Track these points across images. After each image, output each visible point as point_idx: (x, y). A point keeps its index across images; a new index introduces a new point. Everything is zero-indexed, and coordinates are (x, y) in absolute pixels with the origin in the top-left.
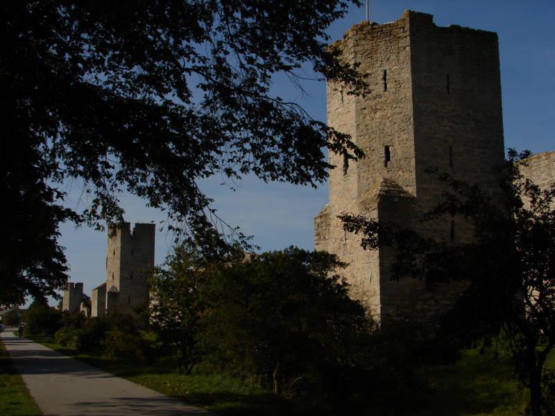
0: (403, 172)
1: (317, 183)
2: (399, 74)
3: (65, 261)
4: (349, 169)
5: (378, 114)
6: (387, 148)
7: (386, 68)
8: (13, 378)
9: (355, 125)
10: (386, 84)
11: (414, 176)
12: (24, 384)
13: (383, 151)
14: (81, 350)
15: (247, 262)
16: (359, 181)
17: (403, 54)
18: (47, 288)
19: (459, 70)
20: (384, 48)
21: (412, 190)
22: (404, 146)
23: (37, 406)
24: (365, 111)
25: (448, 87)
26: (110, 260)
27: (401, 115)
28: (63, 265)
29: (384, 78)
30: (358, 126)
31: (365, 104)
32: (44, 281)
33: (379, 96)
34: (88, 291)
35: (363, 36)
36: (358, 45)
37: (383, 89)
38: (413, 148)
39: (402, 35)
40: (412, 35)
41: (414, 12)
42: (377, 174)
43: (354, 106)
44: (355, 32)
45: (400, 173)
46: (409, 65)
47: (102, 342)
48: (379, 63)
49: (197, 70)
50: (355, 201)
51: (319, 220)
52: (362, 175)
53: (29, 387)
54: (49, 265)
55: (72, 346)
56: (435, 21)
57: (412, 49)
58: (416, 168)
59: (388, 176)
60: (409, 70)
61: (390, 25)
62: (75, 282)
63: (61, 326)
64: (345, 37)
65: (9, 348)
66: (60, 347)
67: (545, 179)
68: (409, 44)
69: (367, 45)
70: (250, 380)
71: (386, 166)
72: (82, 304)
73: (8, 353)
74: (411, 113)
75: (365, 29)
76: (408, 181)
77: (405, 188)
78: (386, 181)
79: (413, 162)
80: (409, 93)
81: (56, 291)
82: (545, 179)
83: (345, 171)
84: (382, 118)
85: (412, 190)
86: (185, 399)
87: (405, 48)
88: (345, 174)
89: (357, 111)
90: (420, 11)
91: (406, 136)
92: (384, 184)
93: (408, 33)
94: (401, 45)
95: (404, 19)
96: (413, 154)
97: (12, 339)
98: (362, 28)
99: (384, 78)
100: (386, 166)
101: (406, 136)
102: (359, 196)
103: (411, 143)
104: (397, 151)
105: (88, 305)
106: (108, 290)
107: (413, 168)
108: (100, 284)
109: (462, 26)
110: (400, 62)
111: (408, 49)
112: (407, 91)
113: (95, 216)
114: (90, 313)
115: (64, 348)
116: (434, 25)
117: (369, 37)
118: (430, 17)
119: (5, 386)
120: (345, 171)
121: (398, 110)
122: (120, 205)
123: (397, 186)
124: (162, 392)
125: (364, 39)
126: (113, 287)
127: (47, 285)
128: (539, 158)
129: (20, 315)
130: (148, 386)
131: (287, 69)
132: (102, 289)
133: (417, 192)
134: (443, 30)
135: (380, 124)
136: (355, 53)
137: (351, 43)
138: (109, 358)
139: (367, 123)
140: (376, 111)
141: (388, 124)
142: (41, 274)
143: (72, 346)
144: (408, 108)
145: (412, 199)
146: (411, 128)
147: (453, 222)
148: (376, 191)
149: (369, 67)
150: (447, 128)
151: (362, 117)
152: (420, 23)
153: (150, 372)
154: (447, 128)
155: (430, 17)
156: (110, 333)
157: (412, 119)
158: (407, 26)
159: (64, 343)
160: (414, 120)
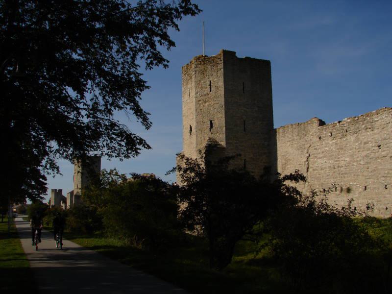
2: (217, 83)
4: (192, 132)
5: (207, 104)
6: (211, 122)
7: (211, 79)
8: (16, 240)
9: (195, 109)
10: (211, 88)
11: (224, 136)
13: (209, 123)
15: (17, 204)
18: (36, 195)
20: (210, 69)
21: (223, 143)
22: (220, 120)
24: (200, 102)
26: (75, 177)
27: (218, 105)
28: (45, 182)
29: (210, 85)
30: (196, 110)
33: (208, 94)
34: (65, 194)
36: (197, 67)
38: (224, 121)
39: (219, 62)
40: (224, 63)
41: (225, 50)
43: (194, 99)
45: (218, 134)
48: (208, 77)
49: (85, 109)
52: (198, 135)
54: (38, 182)
57: (224, 70)
58: (226, 133)
59: (211, 136)
60: (223, 81)
63: (46, 214)
64: (191, 63)
65: (17, 226)
67: (291, 138)
68: (222, 67)
69: (201, 67)
71: (210, 131)
72: (62, 202)
73: (16, 229)
74: (223, 103)
76: (222, 141)
77: (220, 143)
78: (210, 139)
79: (224, 129)
80: (223, 93)
81: (41, 196)
82: (291, 138)
84: (208, 106)
85: (223, 143)
87: (220, 69)
88: (191, 134)
89: (196, 103)
91: (221, 115)
93: (222, 61)
96: (224, 125)
99: (210, 85)
100: (210, 131)
102: (196, 147)
103: (224, 119)
104: (216, 123)
105: (65, 202)
107: (224, 133)
110: (218, 76)
111: (222, 70)
112: (222, 92)
113: (46, 168)
114: (66, 207)
115: (47, 226)
116: (236, 57)
117: (202, 63)
118: (235, 53)
119: (11, 243)
120: (191, 133)
121: (217, 102)
122: (57, 165)
123: (216, 141)
124: (80, 244)
125: (200, 64)
126: (77, 192)
127: (36, 193)
128: (288, 127)
129: (26, 208)
132: (72, 193)
133: (226, 144)
134: (241, 59)
135: (208, 109)
136: (196, 71)
137: (193, 66)
140: (205, 102)
141: (212, 109)
144: (222, 100)
145: (224, 148)
148: (204, 144)
149: (202, 79)
150: (243, 111)
152: (229, 56)
153: (80, 238)
155: (235, 53)
156: (68, 218)
157: (224, 107)
158: (222, 59)
160: (225, 107)
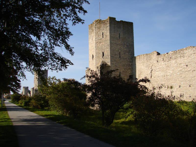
0: (107, 59)
1: (65, 69)
3: (20, 82)
4: (94, 58)
5: (101, 44)
6: (103, 53)
7: (103, 32)
8: (6, 112)
10: (103, 36)
12: (8, 113)
14: (25, 106)
16: (96, 61)
17: (107, 28)
18: (16, 89)
19: (122, 32)
20: (103, 26)
22: (108, 52)
23: (9, 117)
24: (98, 43)
25: (119, 37)
26: (35, 81)
29: (103, 34)
31: (98, 41)
32: (15, 87)
34: (30, 89)
35: (97, 23)
37: (102, 37)
39: (107, 23)
40: (110, 23)
42: (101, 60)
43: (95, 41)
44: (95, 22)
45: (106, 59)
46: (109, 31)
47: (29, 104)
49: (40, 46)
50: (95, 67)
51: (87, 71)
52: (97, 60)
53: (9, 114)
55: (23, 105)
56: (116, 19)
57: (110, 27)
61: (104, 20)
62: (26, 87)
63: (20, 99)
64: (93, 23)
65: (6, 105)
66: (20, 105)
67: (143, 61)
69: (98, 25)
70: (60, 112)
71: (103, 57)
72: (28, 93)
74: (109, 44)
75: (98, 21)
78: (102, 61)
80: (109, 38)
82: (143, 61)
83: (93, 58)
86: (42, 116)
89: (95, 43)
90: (112, 17)
91: (108, 50)
92: (102, 62)
94: (107, 26)
95: (108, 19)
97: (8, 103)
98: (97, 21)
99: (103, 34)
100: (103, 57)
101: (108, 50)
102: (96, 65)
104: (105, 54)
105: (30, 93)
106: (35, 89)
108: (33, 87)
109: (124, 21)
111: (109, 27)
112: (108, 38)
113: (20, 76)
114: (30, 95)
116: (116, 20)
117: (99, 23)
118: (115, 18)
120: (93, 58)
125: (98, 24)
127: (15, 88)
128: (141, 56)
129: (10, 96)
130: (36, 113)
131: (59, 46)
132: (33, 88)
133: (111, 64)
134: (118, 22)
136: (95, 28)
137: (94, 25)
138: (31, 108)
139: (98, 46)
140: (100, 43)
141: (103, 46)
142: (14, 86)
143: (23, 105)
145: (109, 66)
146: (109, 47)
147: (120, 72)
148: (100, 64)
150: (119, 48)
151: (97, 44)
152: (112, 20)
154: (119, 48)
159: (21, 104)
